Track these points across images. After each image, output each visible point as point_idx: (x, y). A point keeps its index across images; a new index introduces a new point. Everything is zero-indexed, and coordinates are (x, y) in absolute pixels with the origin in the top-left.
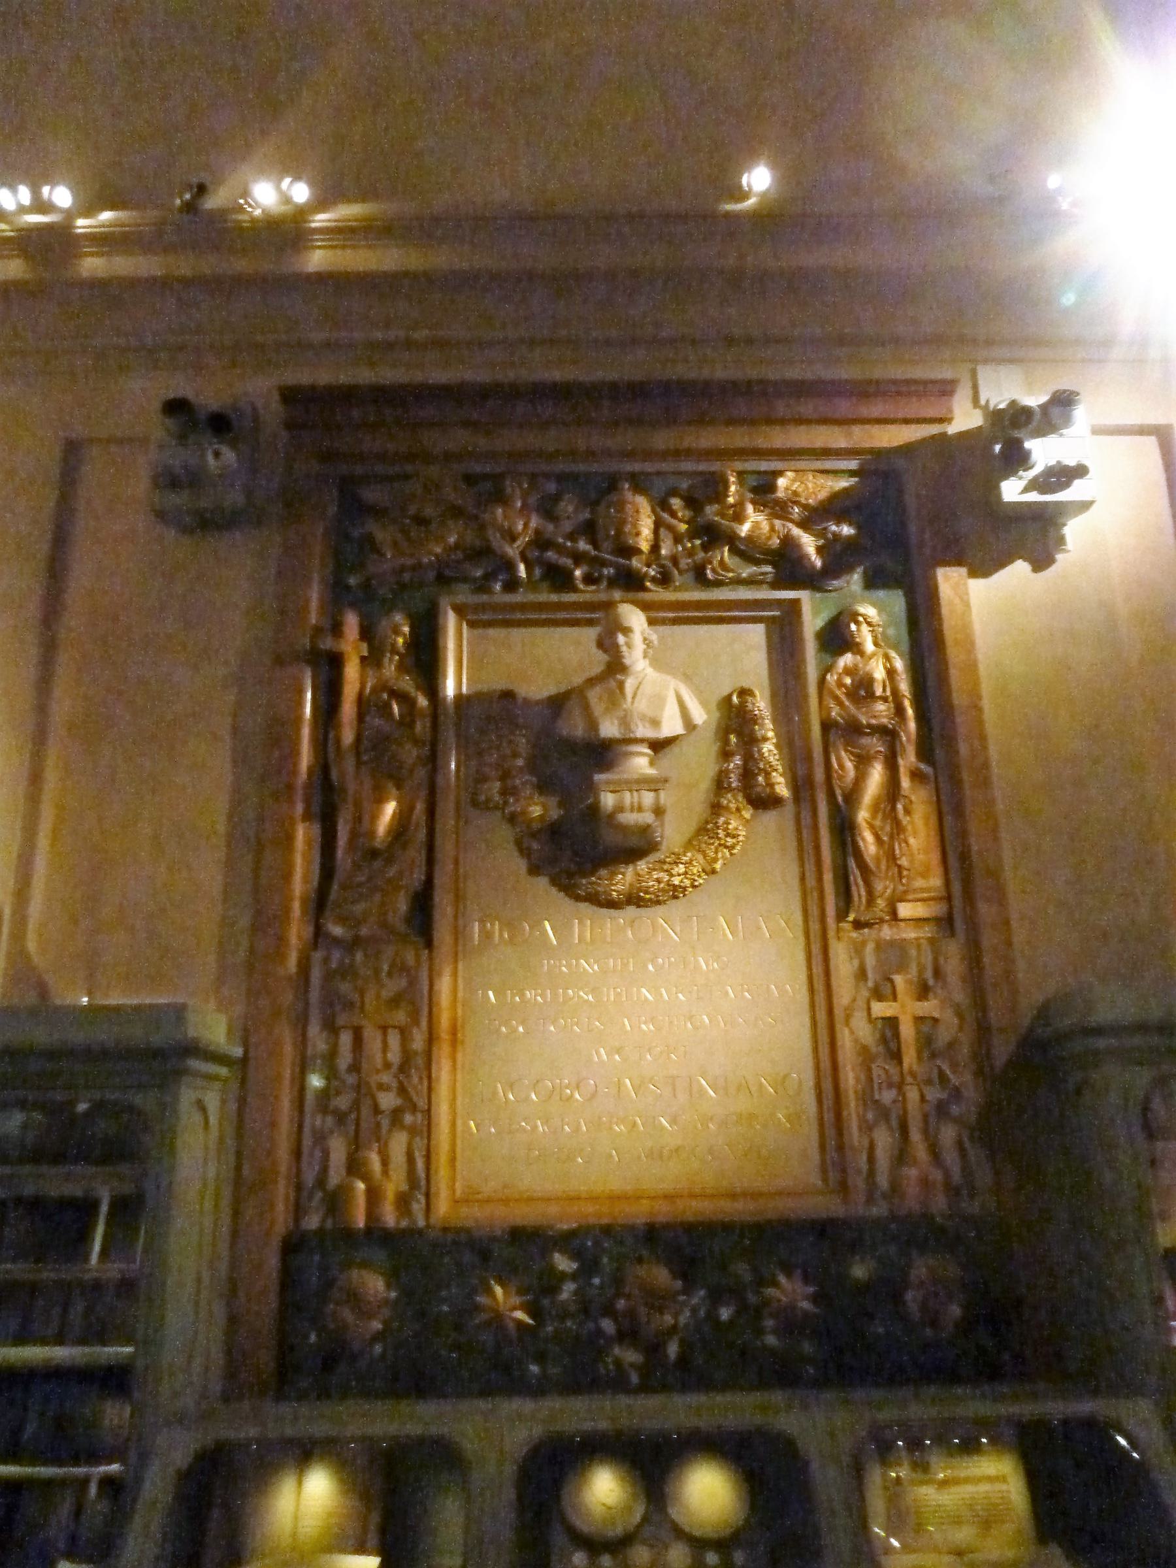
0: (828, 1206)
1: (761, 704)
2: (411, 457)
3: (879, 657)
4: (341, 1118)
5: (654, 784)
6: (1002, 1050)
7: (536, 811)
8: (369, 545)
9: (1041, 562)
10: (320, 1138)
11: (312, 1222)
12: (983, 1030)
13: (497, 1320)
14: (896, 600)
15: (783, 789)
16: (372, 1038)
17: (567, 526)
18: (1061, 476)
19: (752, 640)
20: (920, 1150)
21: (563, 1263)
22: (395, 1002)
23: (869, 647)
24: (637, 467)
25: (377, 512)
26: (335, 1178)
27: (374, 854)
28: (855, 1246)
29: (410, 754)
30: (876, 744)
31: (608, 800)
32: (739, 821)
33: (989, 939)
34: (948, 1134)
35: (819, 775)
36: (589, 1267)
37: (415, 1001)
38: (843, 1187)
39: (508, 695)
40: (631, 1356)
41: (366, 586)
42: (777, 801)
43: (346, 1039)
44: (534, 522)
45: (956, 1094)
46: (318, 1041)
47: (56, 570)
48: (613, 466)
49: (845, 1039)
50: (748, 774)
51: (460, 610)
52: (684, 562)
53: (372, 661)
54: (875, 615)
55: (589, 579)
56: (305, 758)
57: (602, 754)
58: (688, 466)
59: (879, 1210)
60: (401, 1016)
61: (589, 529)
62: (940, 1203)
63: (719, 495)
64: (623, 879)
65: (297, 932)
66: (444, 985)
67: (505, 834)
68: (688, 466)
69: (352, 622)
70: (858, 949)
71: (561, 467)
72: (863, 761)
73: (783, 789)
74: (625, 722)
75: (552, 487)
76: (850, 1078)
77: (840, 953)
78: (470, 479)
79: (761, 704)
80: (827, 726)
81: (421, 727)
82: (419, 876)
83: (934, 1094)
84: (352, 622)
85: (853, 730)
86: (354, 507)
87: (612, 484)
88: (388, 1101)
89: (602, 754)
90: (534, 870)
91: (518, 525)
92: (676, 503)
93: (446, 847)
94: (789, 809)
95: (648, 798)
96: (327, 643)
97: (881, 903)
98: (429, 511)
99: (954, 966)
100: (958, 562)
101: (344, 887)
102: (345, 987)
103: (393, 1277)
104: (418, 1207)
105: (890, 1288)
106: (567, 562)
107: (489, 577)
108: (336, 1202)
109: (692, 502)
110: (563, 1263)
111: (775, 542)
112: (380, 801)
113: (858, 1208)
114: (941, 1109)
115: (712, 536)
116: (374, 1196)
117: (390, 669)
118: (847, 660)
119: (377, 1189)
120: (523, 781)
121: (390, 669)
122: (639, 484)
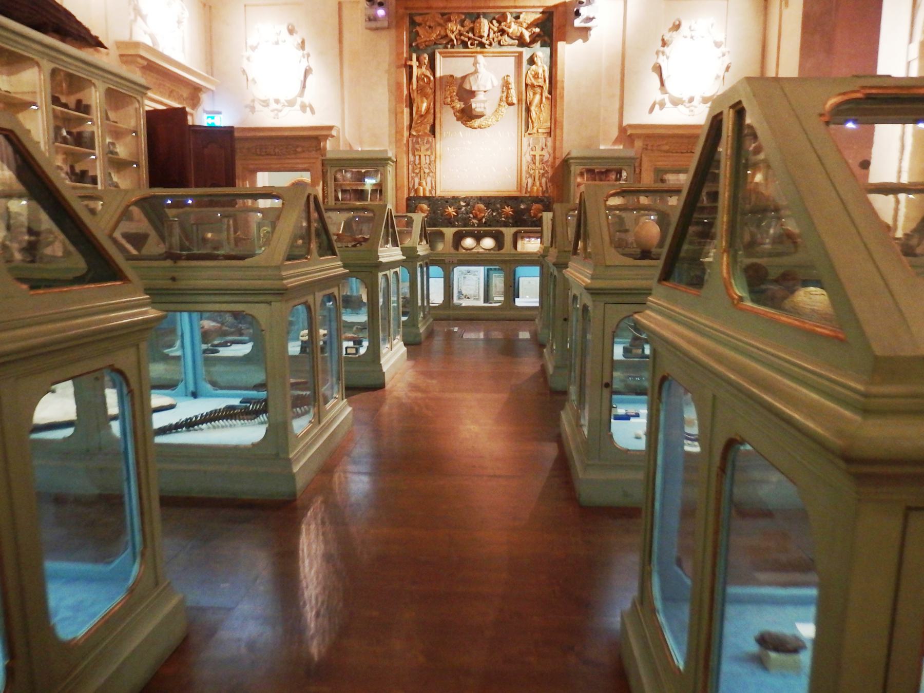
0: (517, 194)
1: (512, 80)
2: (428, 8)
3: (542, 67)
4: (417, 174)
5: (484, 102)
6: (558, 162)
7: (458, 106)
8: (417, 34)
9: (586, 39)
10: (413, 178)
11: (412, 195)
12: (555, 158)
13: (450, 214)
14: (547, 50)
15: (515, 101)
16: (423, 158)
17: (467, 29)
18: (589, 19)
19: (511, 61)
20: (538, 183)
21: (462, 203)
22: (427, 150)
23: (539, 64)
24: (485, 11)
25: (420, 25)
26: (416, 186)
27: (422, 116)
28: (522, 202)
29: (429, 91)
30: (538, 90)
31: (474, 106)
32: (505, 108)
33: (558, 138)
34: (544, 180)
35: (524, 97)
36: (468, 205)
37: (432, 148)
38: (521, 191)
39: (452, 76)
40: (475, 221)
41: (417, 45)
42: (513, 104)
43: (417, 157)
44: (459, 27)
45: (547, 172)
46: (411, 158)
47: (341, 41)
48: (478, 11)
49: (524, 159)
50: (507, 97)
51: (440, 53)
52: (496, 40)
53: (420, 66)
54: (542, 54)
55: (472, 44)
56: (405, 92)
57: (472, 94)
58: (498, 10)
59: (528, 195)
60: (429, 153)
61: (472, 30)
62: (541, 194)
63: (505, 20)
64: (476, 123)
65: (406, 134)
66: (438, 146)
67: (451, 111)
68: (498, 10)
69: (414, 56)
70: (529, 140)
71: (465, 11)
72: (535, 94)
73: (515, 101)
74: (478, 86)
75: (463, 17)
76: (524, 168)
77: (525, 140)
78: (443, 15)
79: (512, 80)
80: (527, 85)
81: (432, 85)
82: (432, 121)
83: (542, 171)
84: (414, 56)
85: (533, 86)
86: (413, 23)
87: (478, 16)
88: (427, 171)
89: (472, 94)
90: (458, 120)
91: (453, 28)
92: (494, 22)
93: (438, 115)
94: (516, 106)
95: (482, 105)
96: (409, 63)
97: (535, 129)
98: (432, 25)
99: (550, 143)
100: (564, 40)
101: (416, 123)
102: (417, 146)
103: (429, 206)
104: (433, 192)
105: (528, 210)
106: (466, 39)
107: (448, 43)
108: (416, 191)
109: (499, 22)
110: (462, 203)
111: (519, 34)
112: (422, 102)
113: (523, 194)
114: (543, 175)
115: (503, 32)
116: (424, 190)
117: (424, 69)
118: (534, 67)
119: (425, 189)
120: (455, 98)
121: (424, 69)
122: (485, 15)
